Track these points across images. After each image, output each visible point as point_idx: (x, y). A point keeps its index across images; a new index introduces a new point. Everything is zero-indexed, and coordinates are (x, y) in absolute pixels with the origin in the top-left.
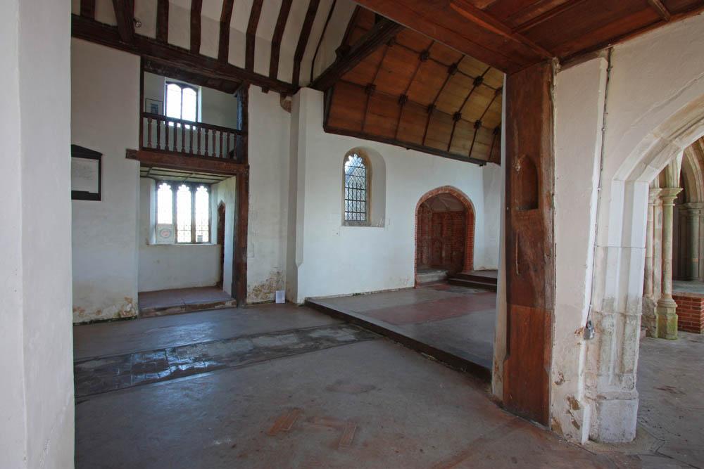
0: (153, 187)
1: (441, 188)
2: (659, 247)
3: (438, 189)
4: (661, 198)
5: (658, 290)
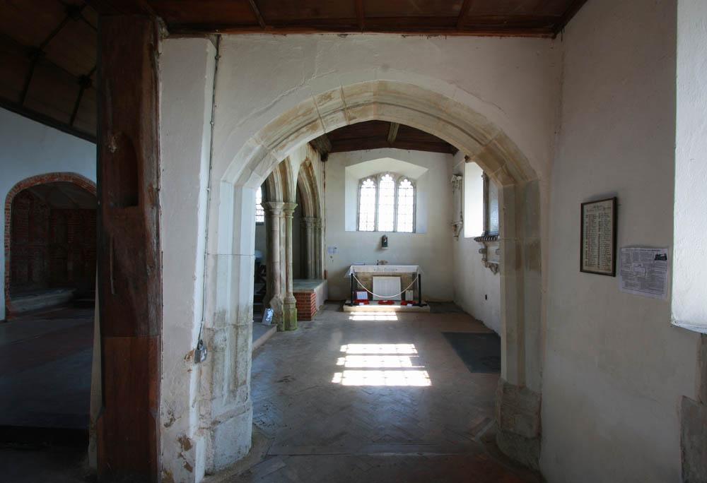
0: (455, 239)
1: (60, 175)
2: (283, 253)
3: (53, 175)
4: (284, 210)
5: (284, 289)
